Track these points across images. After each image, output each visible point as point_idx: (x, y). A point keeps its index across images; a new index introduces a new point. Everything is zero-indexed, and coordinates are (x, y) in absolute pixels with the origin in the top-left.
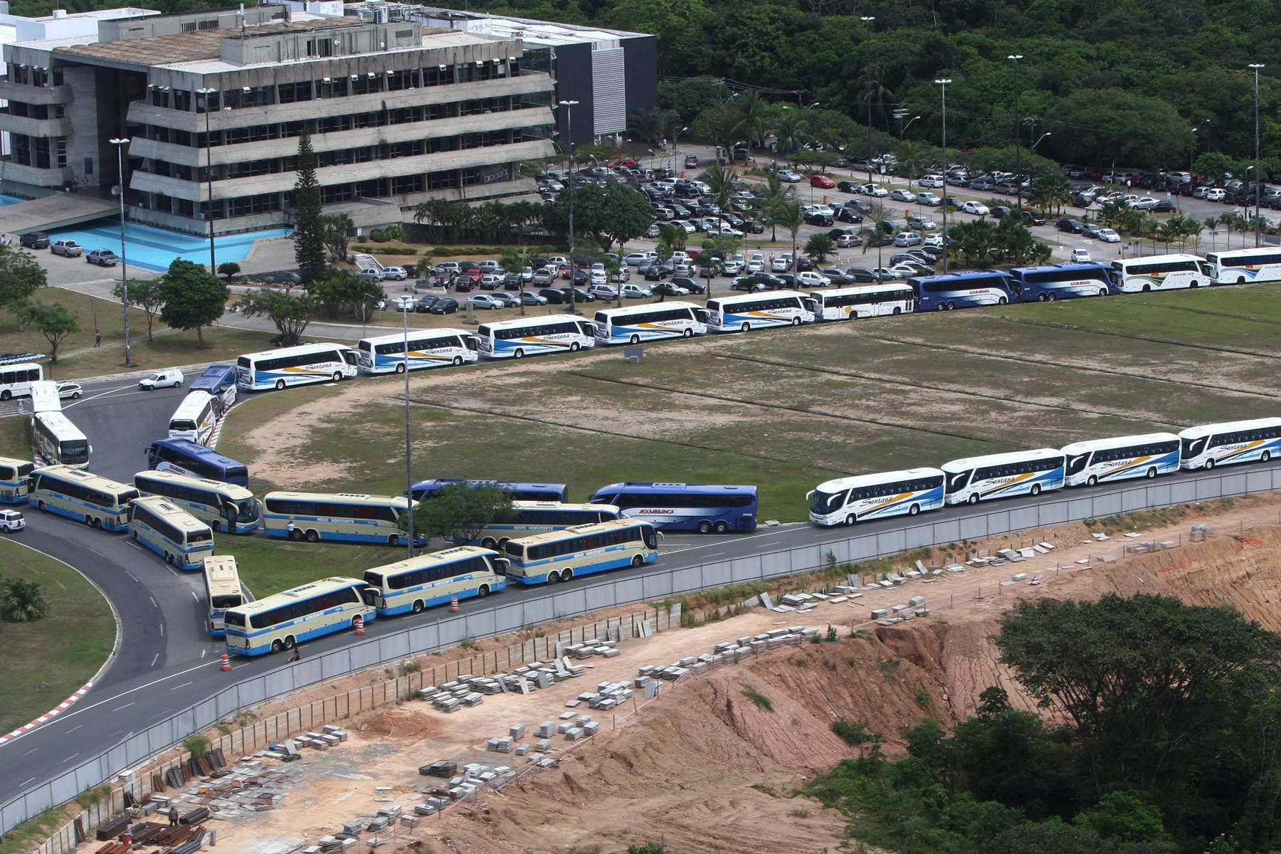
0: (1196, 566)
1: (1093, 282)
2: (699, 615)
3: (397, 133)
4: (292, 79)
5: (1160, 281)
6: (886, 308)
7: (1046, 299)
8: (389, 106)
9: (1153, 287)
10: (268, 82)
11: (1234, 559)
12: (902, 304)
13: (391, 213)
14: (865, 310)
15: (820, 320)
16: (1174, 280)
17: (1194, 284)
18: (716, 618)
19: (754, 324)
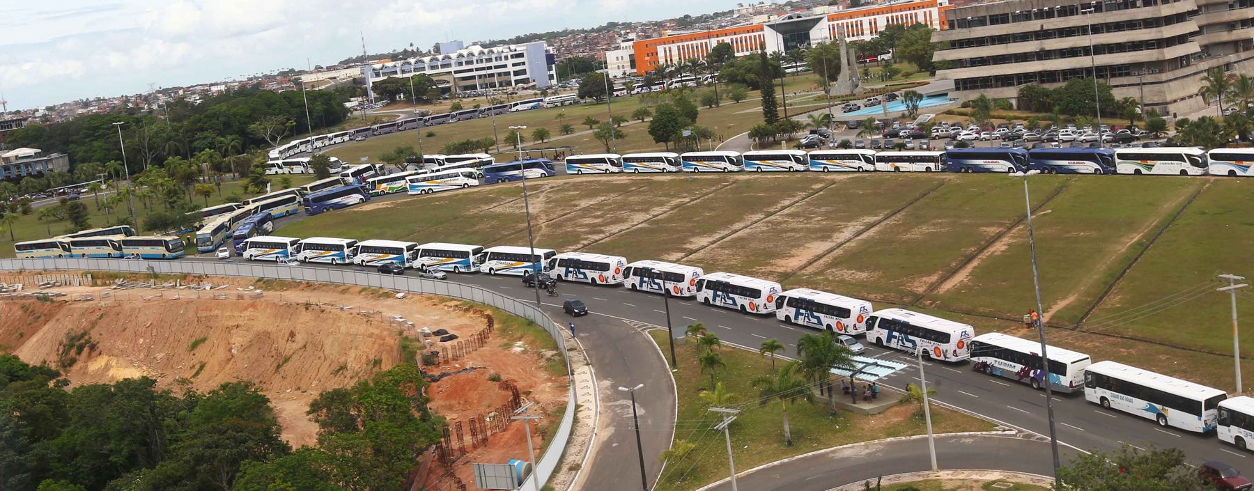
0: (216, 312)
1: (1087, 163)
2: (99, 282)
3: (1031, 46)
4: (997, 12)
5: (1150, 167)
6: (921, 167)
7: (1050, 172)
8: (1045, 27)
9: (1144, 171)
10: (982, 14)
11: (236, 314)
12: (932, 165)
13: (1011, 93)
14: (904, 166)
15: (807, 170)
16: (1160, 168)
17: (1184, 172)
18: (104, 284)
19: (764, 168)
